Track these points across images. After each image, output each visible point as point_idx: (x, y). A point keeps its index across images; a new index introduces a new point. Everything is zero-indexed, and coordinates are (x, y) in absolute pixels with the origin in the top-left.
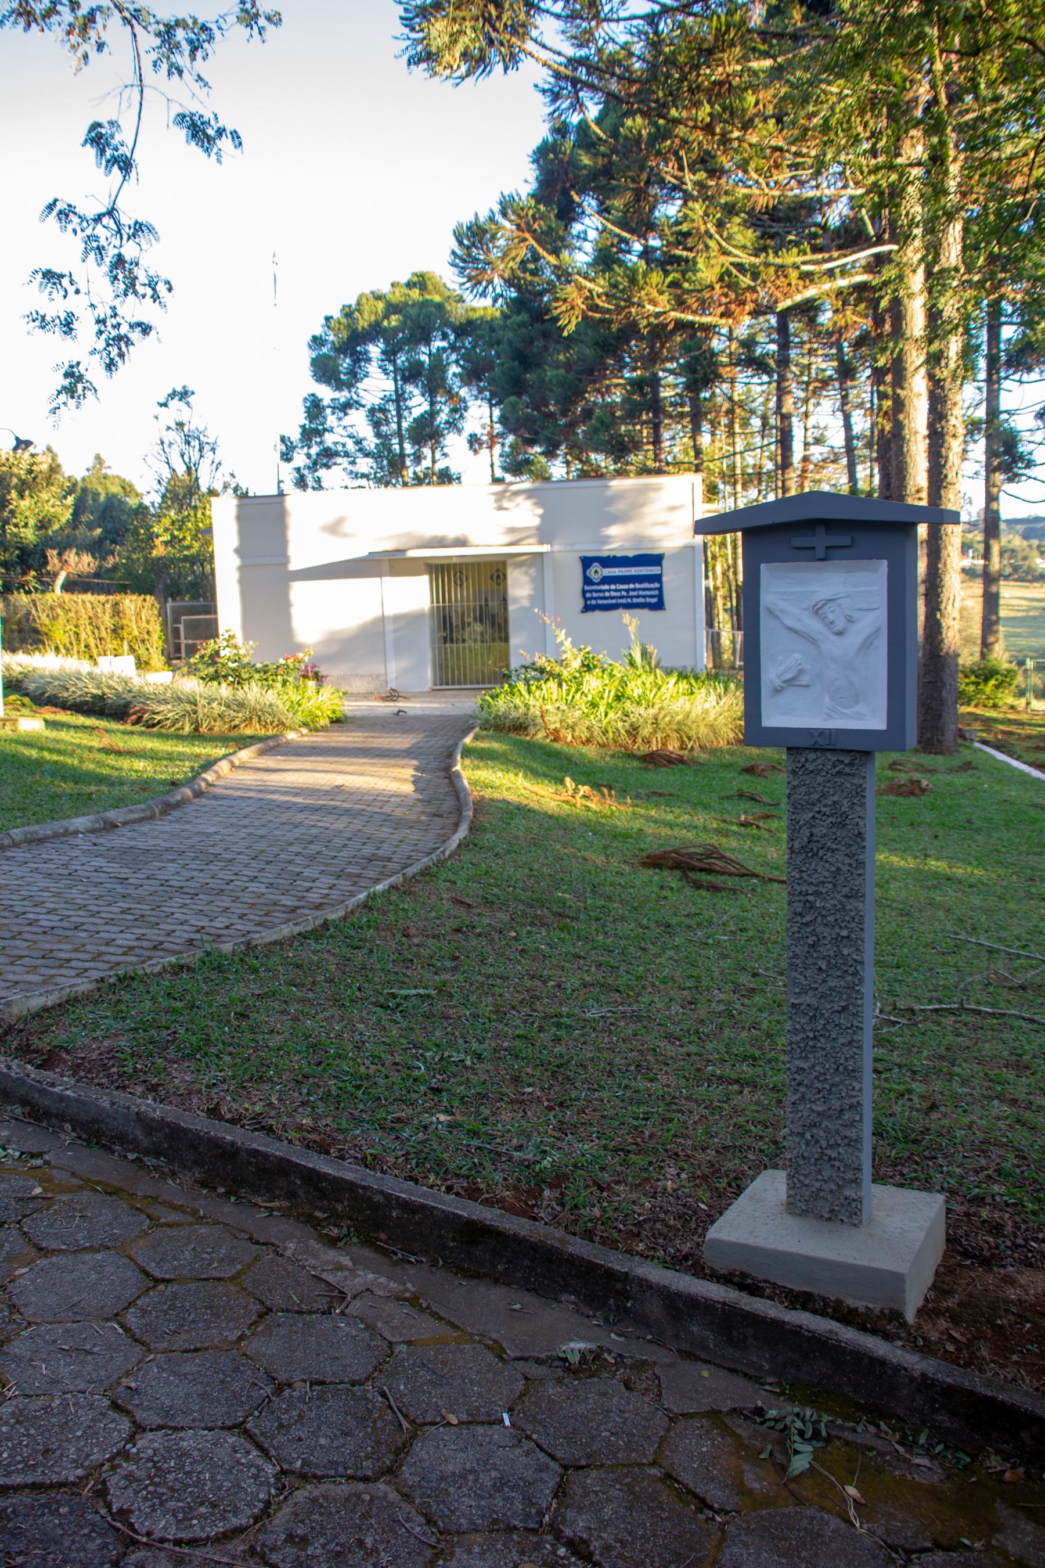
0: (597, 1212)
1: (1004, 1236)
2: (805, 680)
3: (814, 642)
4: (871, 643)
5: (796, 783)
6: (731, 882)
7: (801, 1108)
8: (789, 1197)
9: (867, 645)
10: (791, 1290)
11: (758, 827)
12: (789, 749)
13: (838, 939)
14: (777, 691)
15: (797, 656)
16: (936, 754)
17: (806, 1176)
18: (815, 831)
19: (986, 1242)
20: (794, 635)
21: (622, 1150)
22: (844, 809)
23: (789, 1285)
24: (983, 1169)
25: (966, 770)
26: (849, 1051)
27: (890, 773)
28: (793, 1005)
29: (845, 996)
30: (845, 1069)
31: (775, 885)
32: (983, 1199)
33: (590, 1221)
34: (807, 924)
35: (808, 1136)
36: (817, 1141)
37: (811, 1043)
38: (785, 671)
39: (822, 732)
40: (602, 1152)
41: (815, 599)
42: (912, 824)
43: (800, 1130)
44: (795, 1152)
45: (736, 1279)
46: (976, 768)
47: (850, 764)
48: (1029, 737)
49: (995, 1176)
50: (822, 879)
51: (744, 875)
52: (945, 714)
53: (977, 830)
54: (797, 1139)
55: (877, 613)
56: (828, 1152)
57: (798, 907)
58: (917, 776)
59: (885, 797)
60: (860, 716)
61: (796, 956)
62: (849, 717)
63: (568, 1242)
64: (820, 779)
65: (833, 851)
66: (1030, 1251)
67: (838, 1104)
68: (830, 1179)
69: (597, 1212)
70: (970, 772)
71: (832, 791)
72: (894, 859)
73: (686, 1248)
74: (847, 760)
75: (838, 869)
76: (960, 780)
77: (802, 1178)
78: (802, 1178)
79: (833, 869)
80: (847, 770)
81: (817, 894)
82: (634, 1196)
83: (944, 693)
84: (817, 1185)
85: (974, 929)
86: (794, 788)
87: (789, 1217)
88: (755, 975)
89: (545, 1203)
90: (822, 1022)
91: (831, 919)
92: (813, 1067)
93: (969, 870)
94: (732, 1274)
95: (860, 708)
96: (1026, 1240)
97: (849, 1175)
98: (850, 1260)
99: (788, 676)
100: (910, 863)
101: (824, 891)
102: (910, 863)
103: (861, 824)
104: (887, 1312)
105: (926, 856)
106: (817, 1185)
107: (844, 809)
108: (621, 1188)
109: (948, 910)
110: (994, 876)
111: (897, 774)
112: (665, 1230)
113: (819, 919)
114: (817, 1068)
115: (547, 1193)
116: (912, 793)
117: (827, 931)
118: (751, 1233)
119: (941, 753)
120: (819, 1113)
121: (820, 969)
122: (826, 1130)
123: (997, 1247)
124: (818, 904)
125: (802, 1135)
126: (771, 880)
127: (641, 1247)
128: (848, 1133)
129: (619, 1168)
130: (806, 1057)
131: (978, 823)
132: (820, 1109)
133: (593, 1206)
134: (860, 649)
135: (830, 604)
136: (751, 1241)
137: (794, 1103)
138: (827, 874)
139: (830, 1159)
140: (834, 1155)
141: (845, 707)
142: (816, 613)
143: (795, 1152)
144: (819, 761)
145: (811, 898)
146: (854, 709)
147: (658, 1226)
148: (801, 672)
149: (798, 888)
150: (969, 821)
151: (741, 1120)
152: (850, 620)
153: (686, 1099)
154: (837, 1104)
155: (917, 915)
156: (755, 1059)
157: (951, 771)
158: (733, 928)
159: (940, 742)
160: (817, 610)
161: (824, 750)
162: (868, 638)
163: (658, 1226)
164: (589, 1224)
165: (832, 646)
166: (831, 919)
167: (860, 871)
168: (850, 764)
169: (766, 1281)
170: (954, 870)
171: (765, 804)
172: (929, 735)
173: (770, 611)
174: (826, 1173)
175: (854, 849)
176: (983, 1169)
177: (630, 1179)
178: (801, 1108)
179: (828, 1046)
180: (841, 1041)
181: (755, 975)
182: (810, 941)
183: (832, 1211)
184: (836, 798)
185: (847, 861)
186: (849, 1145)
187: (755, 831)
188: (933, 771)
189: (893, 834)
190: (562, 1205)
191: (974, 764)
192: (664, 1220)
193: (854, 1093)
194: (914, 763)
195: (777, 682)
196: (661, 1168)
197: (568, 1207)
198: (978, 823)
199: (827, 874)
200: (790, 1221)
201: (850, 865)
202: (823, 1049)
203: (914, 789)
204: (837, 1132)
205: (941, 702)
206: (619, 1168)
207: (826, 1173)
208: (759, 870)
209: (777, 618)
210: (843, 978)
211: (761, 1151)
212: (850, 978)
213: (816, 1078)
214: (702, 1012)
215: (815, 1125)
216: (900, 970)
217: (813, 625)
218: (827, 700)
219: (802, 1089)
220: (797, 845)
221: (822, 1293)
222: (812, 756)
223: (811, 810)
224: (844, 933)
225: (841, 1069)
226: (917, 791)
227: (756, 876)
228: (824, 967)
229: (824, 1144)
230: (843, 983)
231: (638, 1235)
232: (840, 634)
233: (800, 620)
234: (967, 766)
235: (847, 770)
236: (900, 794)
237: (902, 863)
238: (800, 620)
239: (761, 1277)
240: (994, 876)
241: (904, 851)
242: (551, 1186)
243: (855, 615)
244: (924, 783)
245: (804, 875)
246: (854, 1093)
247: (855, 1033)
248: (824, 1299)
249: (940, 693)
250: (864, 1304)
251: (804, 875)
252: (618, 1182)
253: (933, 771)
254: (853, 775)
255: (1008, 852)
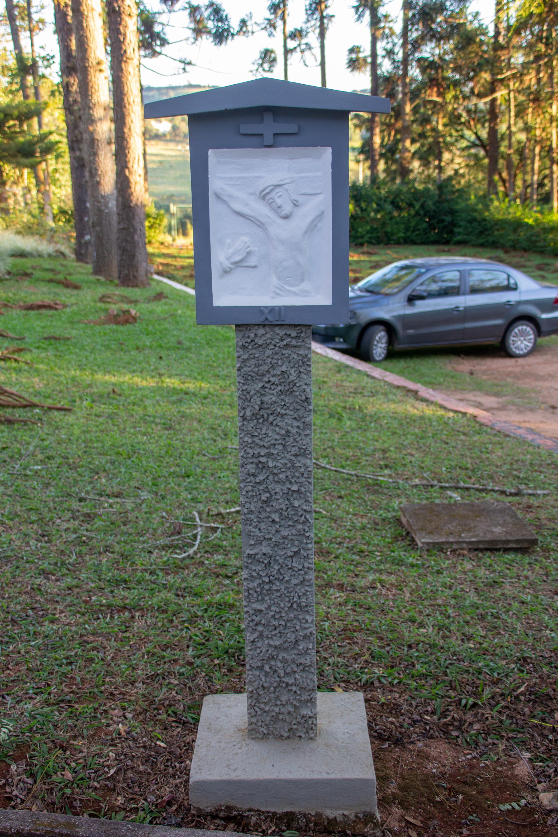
0: (69, 775)
1: (402, 715)
2: (253, 261)
3: (260, 225)
4: (316, 226)
5: (245, 357)
6: (18, 413)
7: (259, 644)
8: (251, 724)
9: (312, 228)
10: (275, 814)
11: (16, 360)
12: (236, 326)
13: (289, 493)
14: (226, 272)
15: (245, 239)
16: (133, 286)
17: (265, 703)
18: (266, 399)
19: (392, 723)
20: (242, 219)
21: (63, 701)
22: (292, 378)
23: (273, 810)
24: (359, 655)
25: (160, 299)
26: (301, 590)
27: (100, 305)
28: (249, 556)
29: (296, 543)
30: (299, 605)
31: (56, 413)
32: (372, 683)
33: (66, 786)
34: (260, 483)
35: (267, 668)
36: (275, 671)
37: (266, 587)
38: (234, 254)
39: (272, 309)
40: (47, 709)
41: (261, 185)
42: (138, 348)
43: (259, 664)
44: (256, 684)
45: (222, 814)
46: (167, 297)
47: (298, 337)
48: (183, 268)
49: (370, 660)
50: (273, 442)
51: (25, 406)
52: (137, 254)
53: (188, 349)
54: (257, 673)
55: (321, 197)
56: (286, 680)
57: (251, 468)
58: (125, 307)
59: (107, 326)
60: (305, 293)
61: (251, 512)
62: (296, 294)
63: (74, 825)
64: (268, 352)
65: (282, 415)
66: (426, 724)
67: (293, 636)
68: (288, 702)
69: (69, 775)
70: (163, 301)
71: (280, 362)
72: (137, 380)
73: (166, 792)
74: (294, 334)
75: (288, 432)
76: (159, 308)
77: (262, 706)
78: (262, 706)
79: (283, 432)
80: (294, 342)
81: (269, 455)
82: (95, 748)
83: (136, 237)
84: (277, 709)
85: (226, 435)
86: (245, 361)
87: (253, 742)
88: (81, 500)
89: (16, 779)
90: (277, 567)
91: (282, 476)
92: (269, 607)
93: (198, 384)
94: (218, 810)
95: (305, 286)
96: (420, 715)
97: (305, 697)
98: (325, 776)
99: (237, 258)
100: (150, 383)
101: (275, 452)
102: (150, 383)
103: (308, 390)
104: (361, 815)
105: (161, 375)
106: (277, 709)
107: (292, 378)
108: (79, 743)
109: (200, 421)
110: (217, 387)
111: (108, 306)
112: (137, 777)
113: (271, 478)
114: (273, 608)
115: (13, 767)
116: (126, 322)
117: (278, 488)
118: (228, 766)
119: (136, 286)
120: (276, 647)
121: (273, 521)
122: (284, 661)
123: (401, 726)
124: (271, 465)
125: (261, 668)
126: (50, 409)
127: (120, 800)
128: (303, 660)
129: (70, 722)
130: (263, 599)
131: (187, 344)
132: (277, 643)
133: (64, 769)
134: (306, 232)
135: (278, 190)
136: (233, 776)
137: (253, 641)
138: (277, 437)
139: (287, 684)
140: (291, 681)
141: (292, 285)
142: (264, 198)
143: (256, 684)
144: (268, 336)
145: (263, 460)
146: (299, 288)
147: (130, 774)
148: (249, 253)
149: (251, 451)
150: (179, 343)
151: (150, 646)
152: (296, 205)
153: (93, 634)
154: (291, 637)
155: (177, 427)
156: (125, 581)
157: (149, 300)
158: (40, 457)
159: (135, 277)
160: (264, 196)
161: (273, 326)
162: (313, 221)
163: (130, 774)
164: (68, 791)
165: (279, 229)
166: (282, 476)
167: (307, 432)
168: (298, 337)
169: (250, 810)
170: (186, 385)
171: (12, 339)
172: (126, 272)
173: (218, 196)
174: (284, 698)
175: (301, 413)
176: (359, 655)
177: (85, 731)
178: (259, 644)
179: (283, 587)
180: (294, 581)
181: (81, 500)
182: (264, 498)
183: (290, 730)
184: (284, 368)
185: (296, 424)
186: (303, 670)
187: (14, 365)
188: (135, 302)
189: (126, 358)
190: (32, 775)
191: (165, 294)
192: (133, 768)
193: (306, 625)
194: (118, 296)
195: (227, 264)
196: (106, 711)
197: (39, 777)
198: (187, 344)
199: (277, 437)
200: (256, 747)
201: (298, 427)
202: (277, 591)
203: (125, 319)
204: (293, 661)
205: (134, 244)
206: (70, 722)
207: (284, 698)
208: (36, 400)
209: (225, 202)
210: (293, 526)
211: (181, 674)
212: (300, 527)
213: (273, 616)
214: (59, 544)
215: (273, 657)
216: (191, 479)
217: (261, 210)
218: (274, 280)
219: (260, 628)
220: (248, 413)
221: (303, 810)
222: (261, 331)
223: (261, 381)
224: (295, 488)
225: (295, 606)
226: (131, 320)
227: (35, 406)
228: (277, 519)
229: (282, 673)
230: (294, 532)
231: (114, 790)
232: (286, 217)
233: (247, 205)
234: (159, 296)
235: (294, 342)
236: (117, 323)
237: (144, 383)
238: (247, 205)
239: (246, 807)
240: (217, 387)
241: (141, 372)
242: (16, 759)
243: (300, 199)
244: (133, 312)
245: (256, 439)
246: (306, 625)
247: (306, 573)
248: (305, 816)
249: (133, 238)
250: (341, 812)
251: (256, 439)
252: (75, 737)
253: (135, 302)
254: (299, 347)
255: (218, 366)
